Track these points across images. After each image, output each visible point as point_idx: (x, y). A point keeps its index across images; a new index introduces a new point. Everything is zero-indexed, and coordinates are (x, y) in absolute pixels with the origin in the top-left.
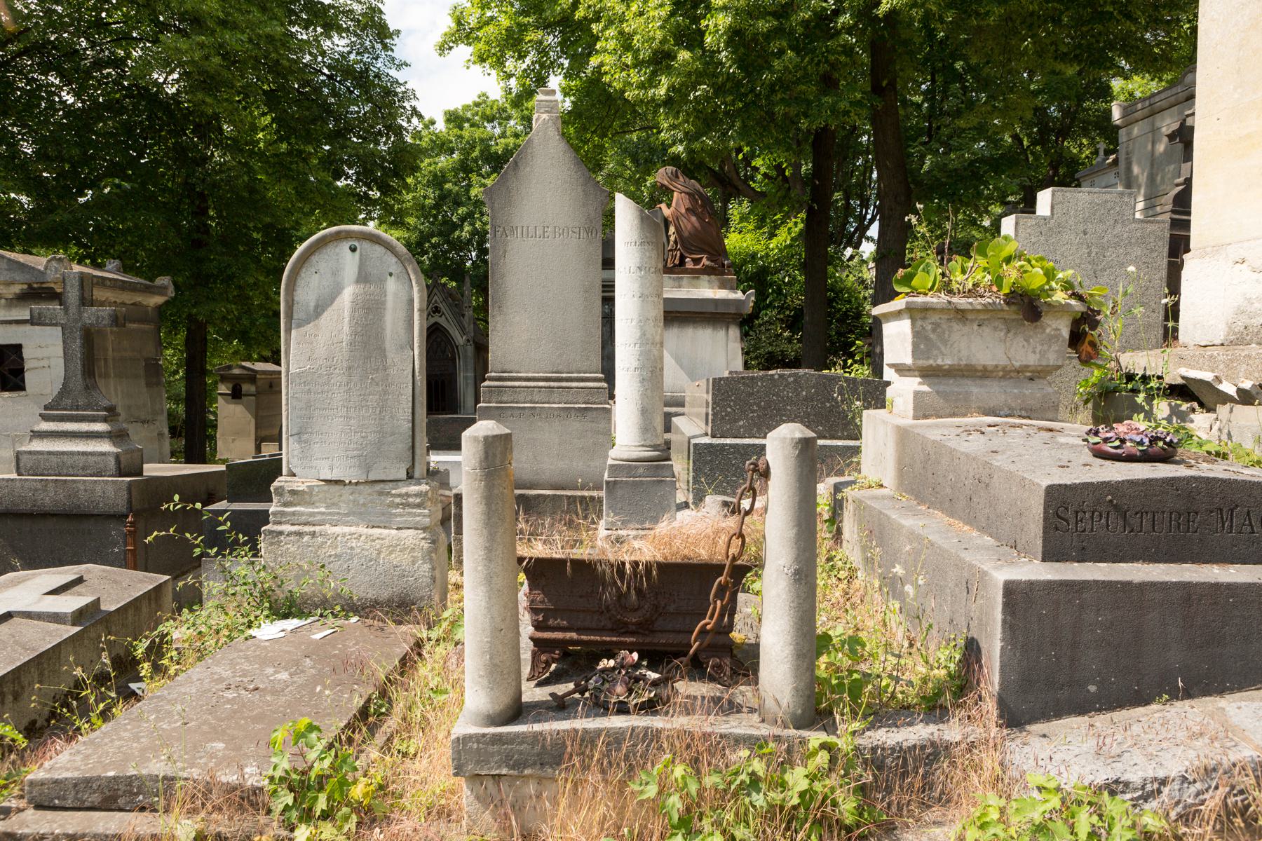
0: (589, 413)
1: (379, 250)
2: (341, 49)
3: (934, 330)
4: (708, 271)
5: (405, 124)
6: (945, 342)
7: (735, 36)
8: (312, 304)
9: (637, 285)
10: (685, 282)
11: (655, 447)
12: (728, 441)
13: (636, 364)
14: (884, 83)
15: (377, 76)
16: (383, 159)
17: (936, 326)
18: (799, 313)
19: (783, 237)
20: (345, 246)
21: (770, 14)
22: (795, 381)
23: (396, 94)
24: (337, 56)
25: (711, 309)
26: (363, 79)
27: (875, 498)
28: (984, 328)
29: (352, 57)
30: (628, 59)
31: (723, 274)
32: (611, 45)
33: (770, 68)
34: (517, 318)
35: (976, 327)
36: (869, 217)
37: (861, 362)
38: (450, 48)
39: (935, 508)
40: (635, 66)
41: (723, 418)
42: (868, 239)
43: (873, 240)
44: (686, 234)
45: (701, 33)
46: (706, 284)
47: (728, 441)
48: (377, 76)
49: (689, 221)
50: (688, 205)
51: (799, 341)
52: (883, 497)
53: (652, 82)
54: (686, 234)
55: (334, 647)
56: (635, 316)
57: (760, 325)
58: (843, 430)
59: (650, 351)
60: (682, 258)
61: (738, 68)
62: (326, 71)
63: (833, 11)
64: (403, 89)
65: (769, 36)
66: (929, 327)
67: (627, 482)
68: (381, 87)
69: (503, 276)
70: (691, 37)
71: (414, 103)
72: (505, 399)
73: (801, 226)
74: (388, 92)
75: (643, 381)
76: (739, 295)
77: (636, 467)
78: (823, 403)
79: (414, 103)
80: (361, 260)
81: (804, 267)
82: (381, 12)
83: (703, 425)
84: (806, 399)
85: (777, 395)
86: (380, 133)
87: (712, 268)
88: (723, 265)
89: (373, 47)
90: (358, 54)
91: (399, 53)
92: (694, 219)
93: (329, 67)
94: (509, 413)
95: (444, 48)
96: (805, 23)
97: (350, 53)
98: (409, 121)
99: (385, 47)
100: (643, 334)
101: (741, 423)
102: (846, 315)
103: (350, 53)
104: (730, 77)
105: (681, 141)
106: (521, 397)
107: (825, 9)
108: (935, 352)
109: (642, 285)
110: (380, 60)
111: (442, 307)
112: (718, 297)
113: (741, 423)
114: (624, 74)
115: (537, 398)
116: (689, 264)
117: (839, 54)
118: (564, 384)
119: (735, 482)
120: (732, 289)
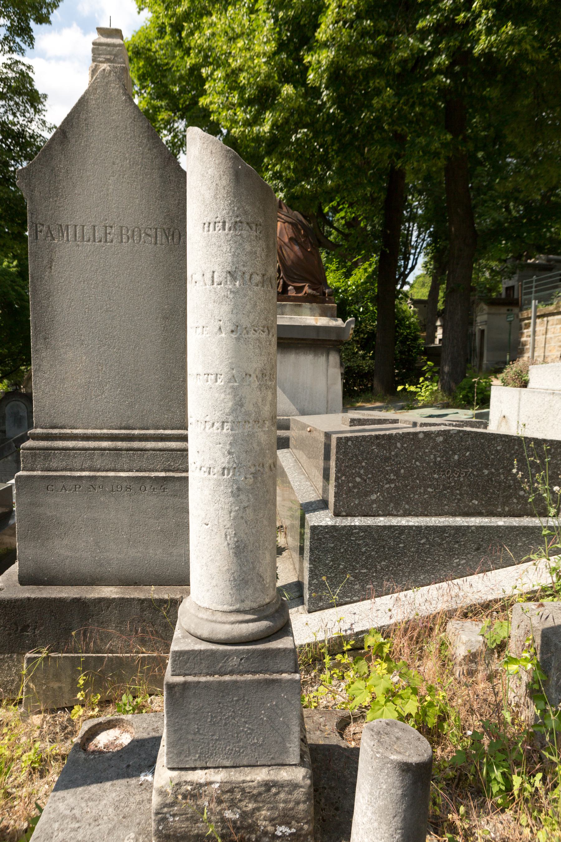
0: (170, 485)
4: (309, 299)
7: (336, 75)
9: (226, 308)
10: (287, 309)
11: (260, 613)
12: (357, 521)
13: (223, 461)
18: (372, 335)
19: (359, 275)
21: (370, 53)
22: (445, 441)
25: (313, 336)
30: (235, 98)
31: (324, 302)
32: (220, 85)
33: (370, 107)
34: (70, 355)
37: (431, 380)
40: (240, 105)
41: (350, 490)
44: (289, 263)
45: (305, 69)
46: (308, 311)
47: (357, 521)
49: (292, 250)
50: (291, 234)
51: (372, 358)
53: (256, 120)
54: (289, 263)
56: (223, 369)
58: (504, 504)
59: (251, 435)
60: (285, 286)
61: (338, 108)
63: (429, 52)
65: (371, 72)
67: (207, 685)
70: (295, 74)
72: (54, 465)
73: (374, 266)
75: (237, 492)
76: (339, 322)
77: (226, 655)
78: (480, 470)
81: (375, 300)
83: (319, 482)
84: (459, 463)
85: (422, 460)
87: (314, 296)
88: (324, 294)
92: (296, 248)
94: (60, 484)
96: (404, 62)
99: (37, 111)
100: (239, 404)
101: (374, 497)
102: (406, 338)
104: (330, 117)
105: (282, 190)
106: (77, 463)
107: (422, 51)
109: (236, 309)
110: (34, 123)
112: (319, 324)
113: (374, 497)
114: (231, 112)
115: (98, 464)
116: (292, 292)
118: (136, 444)
119: (366, 575)
120: (332, 316)
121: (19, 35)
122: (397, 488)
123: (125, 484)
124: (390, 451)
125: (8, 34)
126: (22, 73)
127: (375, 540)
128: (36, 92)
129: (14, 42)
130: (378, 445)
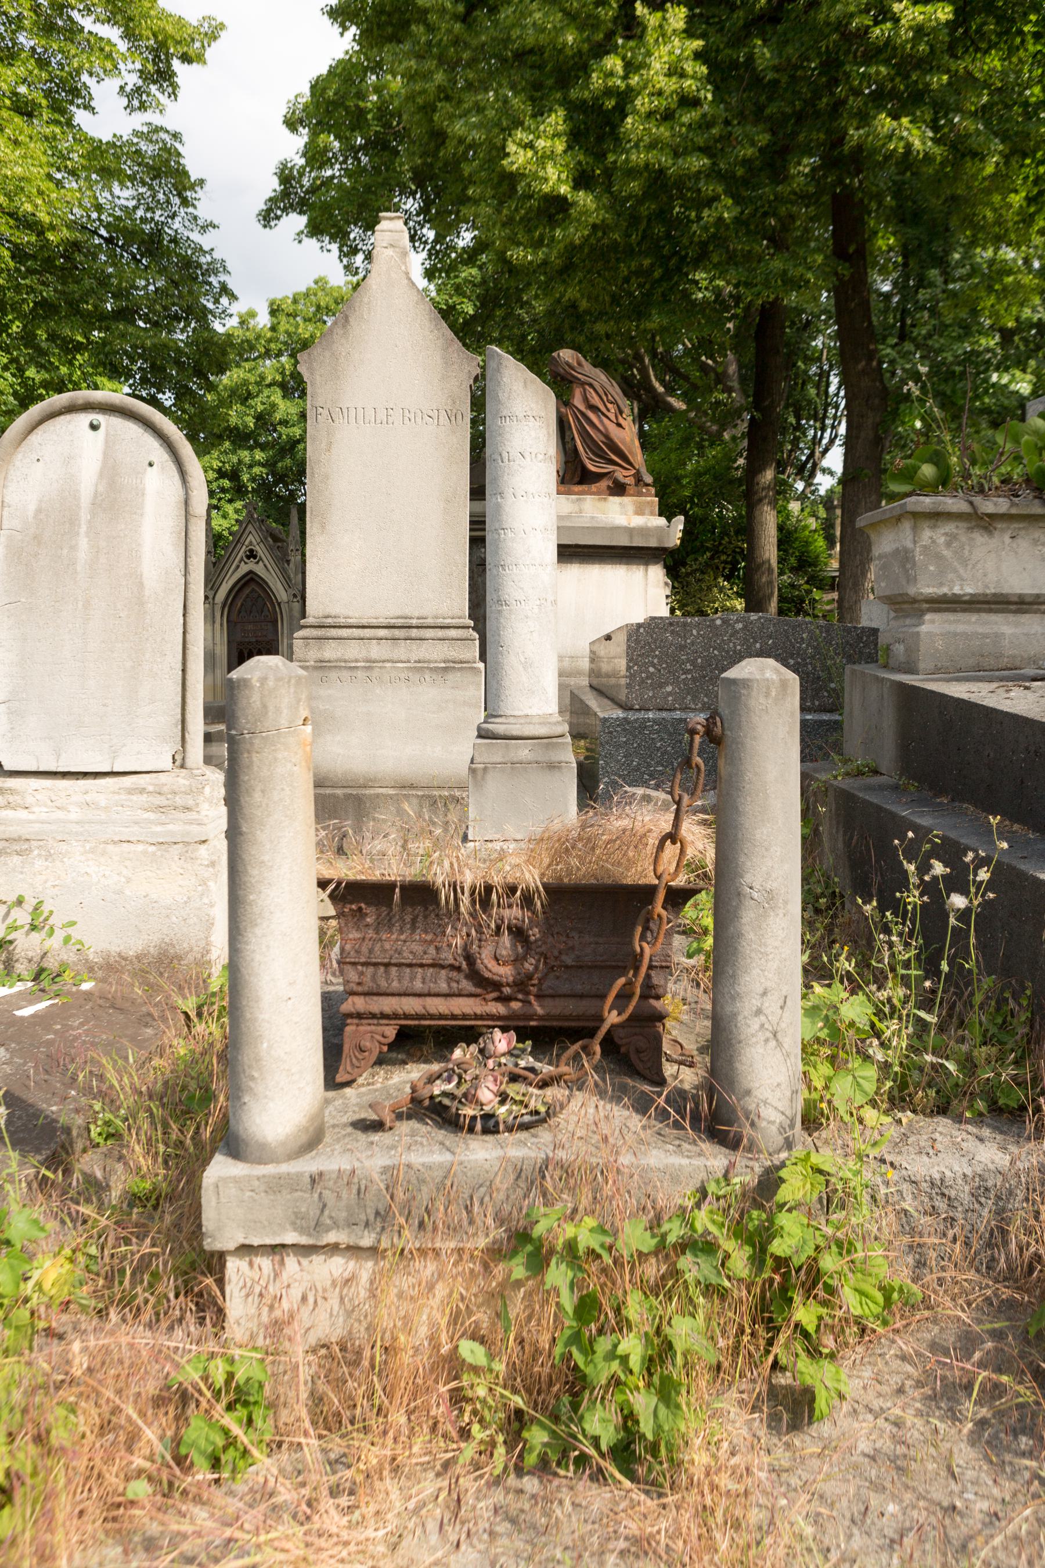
1: (133, 429)
2: (123, 202)
3: (948, 544)
5: (210, 306)
6: (965, 562)
8: (32, 507)
14: (851, 250)
15: (174, 240)
16: (178, 350)
17: (952, 538)
20: (84, 419)
22: (745, 627)
23: (199, 266)
24: (118, 213)
25: (624, 541)
26: (154, 245)
27: (869, 788)
28: (1019, 541)
29: (140, 213)
35: (1007, 539)
36: (825, 441)
38: (278, 218)
39: (962, 801)
42: (824, 471)
43: (831, 473)
48: (174, 240)
52: (881, 788)
55: (48, 1029)
57: (688, 575)
62: (103, 232)
64: (209, 258)
66: (942, 540)
68: (178, 255)
69: (327, 477)
71: (222, 277)
74: (188, 263)
79: (222, 277)
80: (107, 442)
82: (179, 155)
85: (720, 648)
86: (177, 318)
89: (168, 202)
90: (148, 209)
91: (204, 210)
93: (108, 226)
95: (268, 217)
97: (136, 208)
98: (217, 301)
99: (185, 202)
101: (669, 689)
103: (136, 208)
108: (951, 576)
110: (178, 219)
111: (260, 550)
113: (669, 689)
117: (792, 203)
121: (155, 82)
122: (694, 679)
123: (403, 676)
124: (685, 638)
125: (140, 83)
126: (165, 149)
127: (670, 734)
128: (185, 174)
129: (148, 95)
130: (672, 632)
